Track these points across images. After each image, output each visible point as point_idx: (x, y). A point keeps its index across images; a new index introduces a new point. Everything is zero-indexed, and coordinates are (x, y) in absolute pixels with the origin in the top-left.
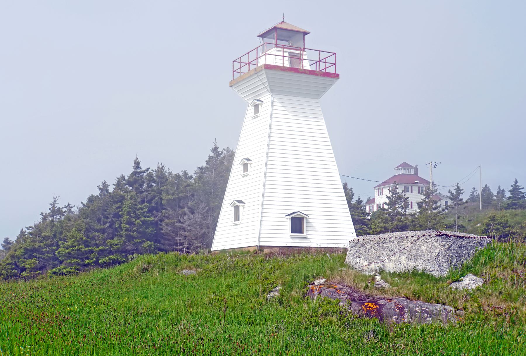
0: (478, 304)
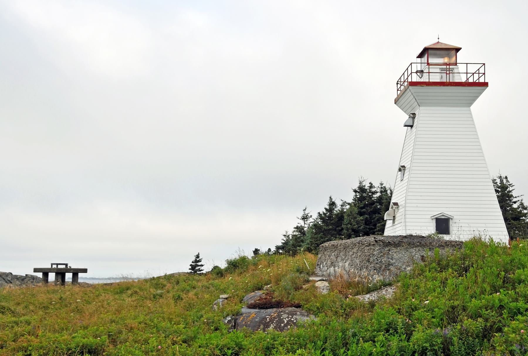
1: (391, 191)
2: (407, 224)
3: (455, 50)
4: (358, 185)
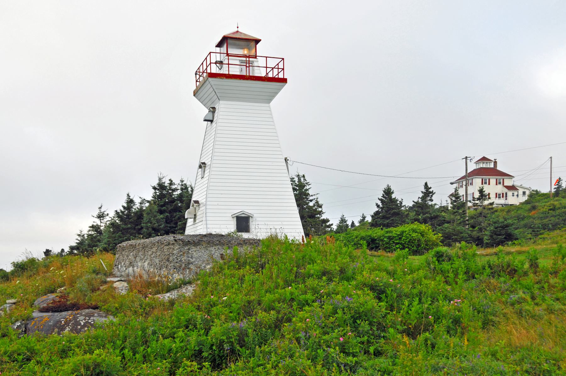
0: (520, 289)
1: (192, 188)
2: (208, 222)
3: (254, 41)
4: (157, 182)
